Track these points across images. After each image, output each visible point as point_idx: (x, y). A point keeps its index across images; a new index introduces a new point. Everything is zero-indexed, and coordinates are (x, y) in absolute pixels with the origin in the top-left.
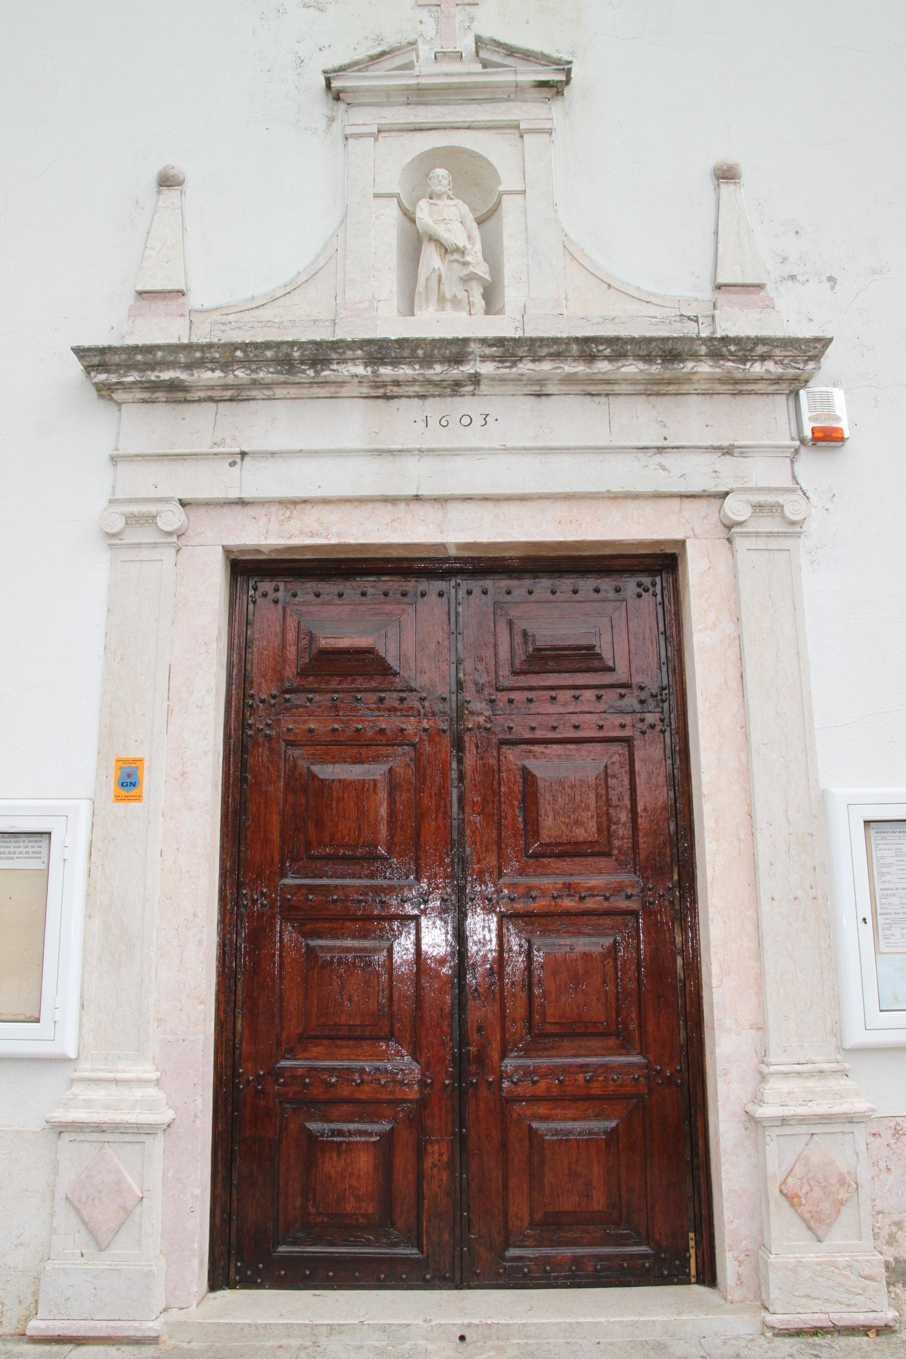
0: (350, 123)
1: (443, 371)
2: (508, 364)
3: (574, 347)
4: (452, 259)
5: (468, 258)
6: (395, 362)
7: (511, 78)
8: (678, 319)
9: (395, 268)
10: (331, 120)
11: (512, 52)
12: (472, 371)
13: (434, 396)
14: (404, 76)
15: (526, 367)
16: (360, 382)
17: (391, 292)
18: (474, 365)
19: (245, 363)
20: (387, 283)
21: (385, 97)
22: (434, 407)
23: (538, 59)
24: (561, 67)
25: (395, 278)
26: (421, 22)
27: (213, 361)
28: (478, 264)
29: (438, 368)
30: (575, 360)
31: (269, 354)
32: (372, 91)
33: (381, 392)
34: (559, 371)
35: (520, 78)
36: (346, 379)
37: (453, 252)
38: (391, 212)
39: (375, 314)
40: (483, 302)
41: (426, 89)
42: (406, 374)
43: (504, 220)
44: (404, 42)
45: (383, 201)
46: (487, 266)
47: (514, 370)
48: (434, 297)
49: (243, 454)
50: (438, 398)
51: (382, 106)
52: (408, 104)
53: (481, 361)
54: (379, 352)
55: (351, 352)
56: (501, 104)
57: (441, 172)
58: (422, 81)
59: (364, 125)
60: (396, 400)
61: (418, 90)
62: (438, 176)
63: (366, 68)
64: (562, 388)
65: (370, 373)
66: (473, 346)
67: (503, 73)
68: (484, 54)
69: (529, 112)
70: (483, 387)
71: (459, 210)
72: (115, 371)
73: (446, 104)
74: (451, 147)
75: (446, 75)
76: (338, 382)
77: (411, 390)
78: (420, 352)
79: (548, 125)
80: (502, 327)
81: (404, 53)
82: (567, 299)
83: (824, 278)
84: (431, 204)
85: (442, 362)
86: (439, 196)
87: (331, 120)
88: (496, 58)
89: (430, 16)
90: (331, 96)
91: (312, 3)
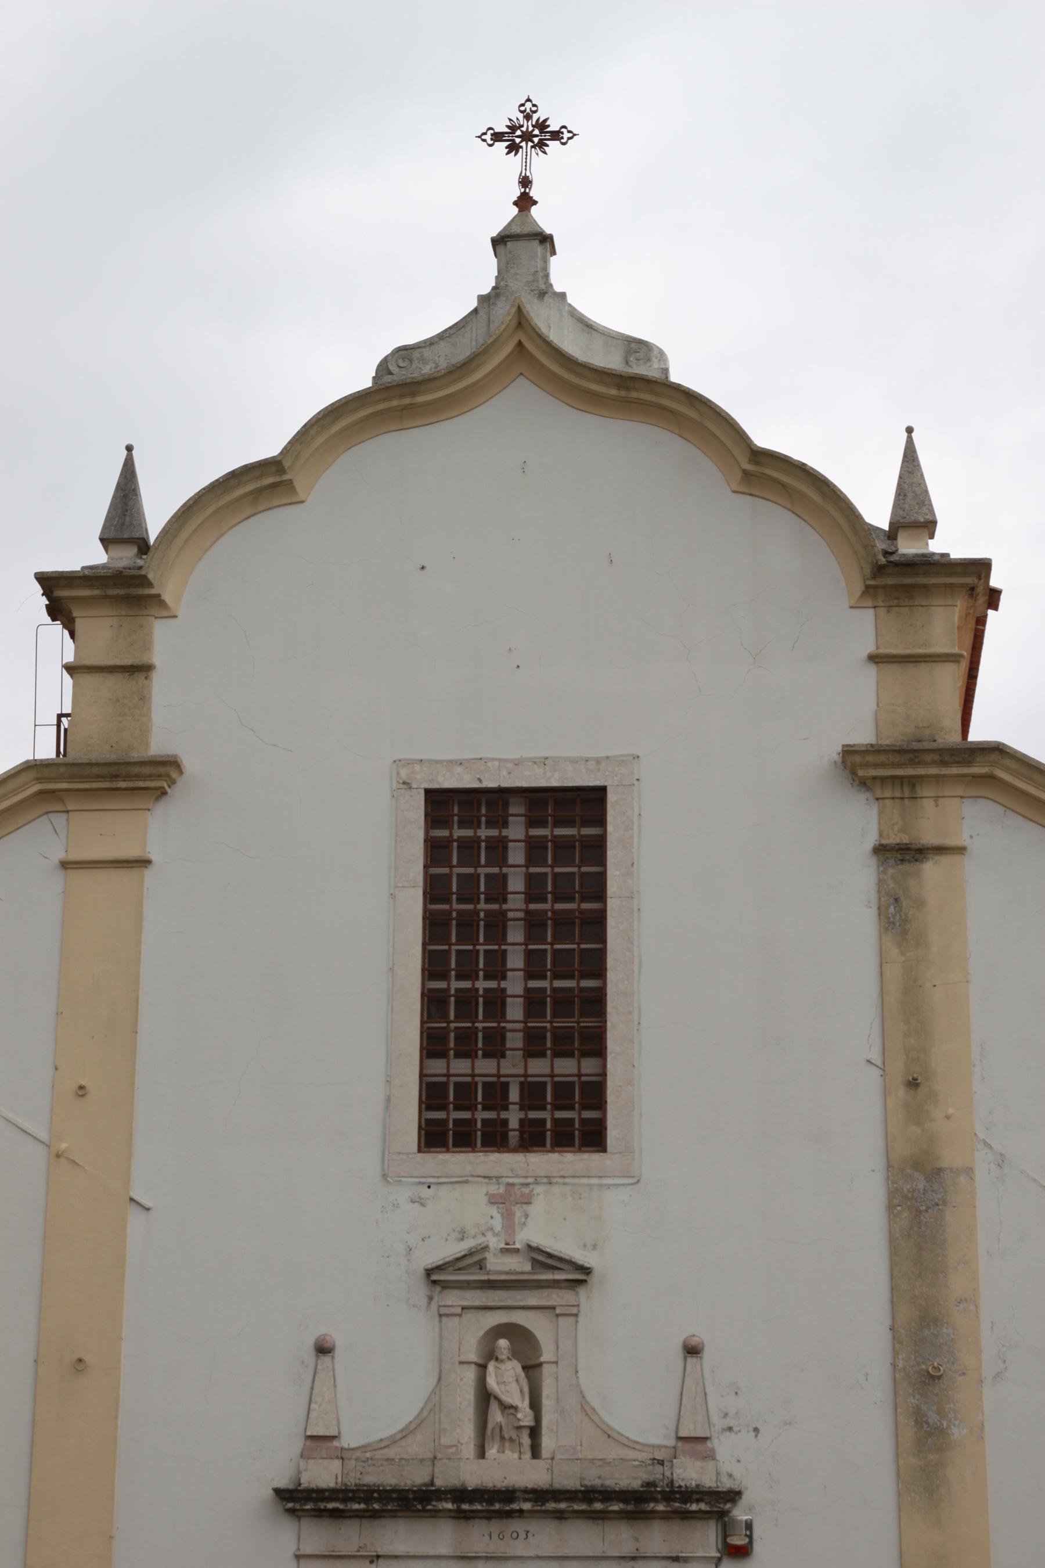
5: (519, 1416)
6: (471, 1502)
8: (650, 1462)
10: (430, 1298)
15: (551, 1506)
19: (379, 1500)
22: (495, 1526)
27: (360, 1498)
31: (394, 1495)
38: (470, 1375)
45: (465, 1366)
48: (497, 1438)
49: (378, 1557)
54: (460, 1494)
69: (558, 1298)
72: (297, 1501)
77: (481, 1515)
79: (574, 1311)
83: (751, 1429)
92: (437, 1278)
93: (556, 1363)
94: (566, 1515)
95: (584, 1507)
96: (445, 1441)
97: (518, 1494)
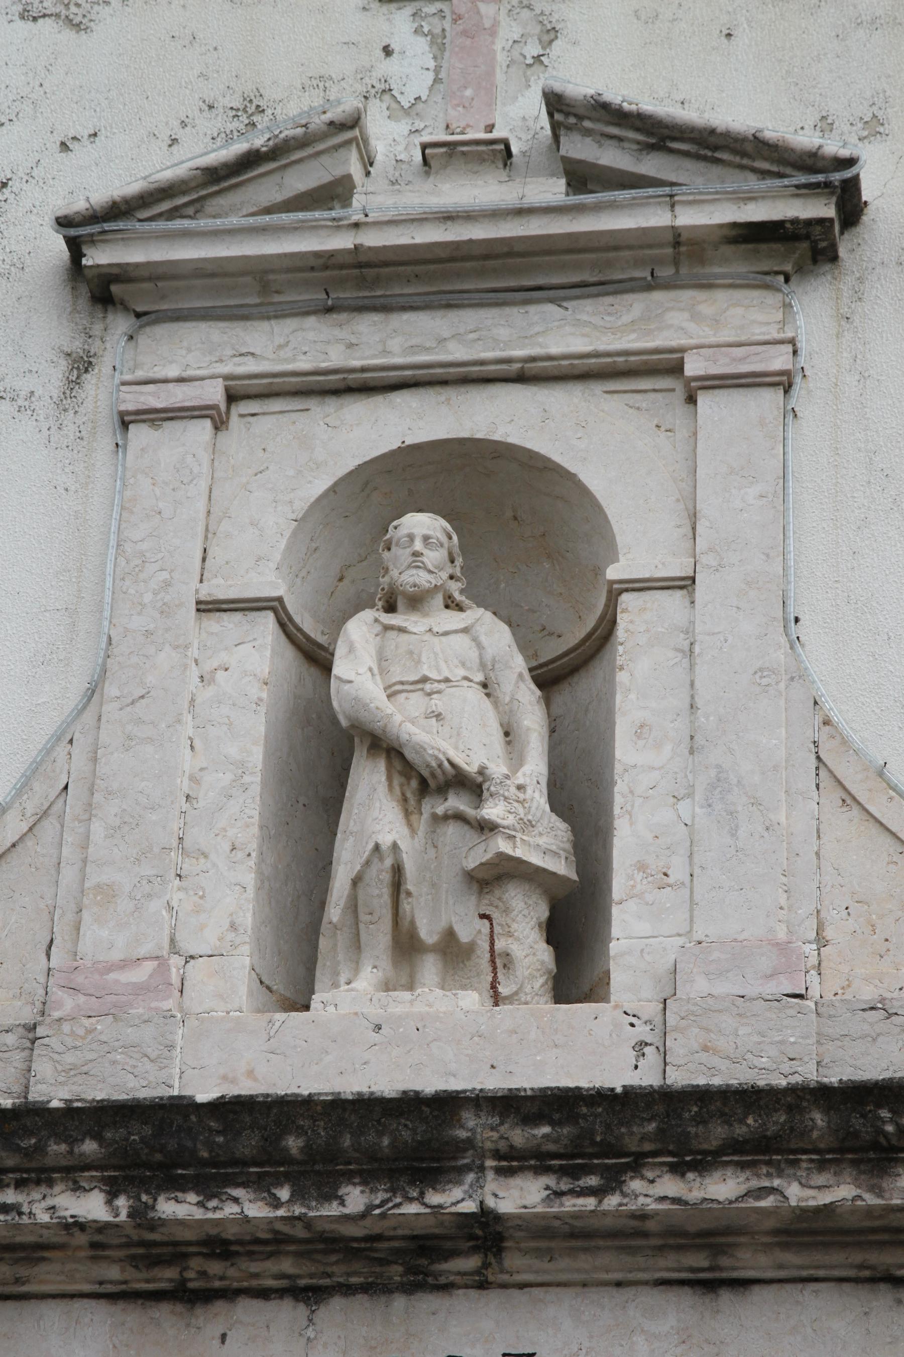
0: (140, 374)
1: (370, 1208)
2: (593, 1181)
3: (819, 1118)
4: (440, 810)
5: (493, 811)
6: (210, 1182)
7: (655, 218)
9: (253, 846)
10: (82, 365)
11: (663, 139)
12: (469, 1207)
13: (347, 1290)
14: (313, 228)
15: (654, 1191)
16: (94, 1245)
17: (233, 927)
18: (479, 1184)
20: (225, 901)
21: (256, 291)
23: (744, 154)
24: (820, 178)
25: (249, 879)
26: (387, 51)
28: (528, 825)
29: (355, 1199)
30: (822, 1166)
32: (213, 275)
33: (167, 1276)
34: (767, 1202)
35: (689, 218)
36: (48, 1236)
37: (443, 790)
38: (255, 656)
39: (169, 1004)
40: (545, 954)
41: (386, 264)
42: (247, 1220)
43: (622, 677)
44: (318, 122)
45: (230, 622)
46: (562, 826)
47: (612, 1201)
48: (379, 937)
50: (361, 1299)
51: (246, 318)
52: (329, 310)
53: (499, 1171)
54: (156, 1141)
55: (63, 1147)
56: (629, 298)
57: (421, 524)
58: (372, 239)
59: (181, 380)
60: (220, 1306)
61: (360, 266)
62: (411, 538)
63: (197, 207)
64: (789, 1257)
65: (123, 1216)
66: (471, 1124)
67: (631, 205)
68: (579, 148)
70: (513, 1260)
71: (479, 646)
73: (449, 306)
74: (461, 441)
75: (448, 217)
76: (23, 1247)
77: (270, 1270)
78: (293, 1144)
79: (779, 360)
80: (584, 1052)
81: (318, 154)
82: (821, 941)
84: (387, 628)
85: (367, 1178)
86: (416, 601)
87: (82, 365)
88: (612, 157)
89: (418, 31)
90: (84, 290)
91: (49, 5)
92: (108, 276)
93: (686, 584)
94: (749, 1262)
95: (841, 1191)
96: (102, 938)
97: (471, 1124)
